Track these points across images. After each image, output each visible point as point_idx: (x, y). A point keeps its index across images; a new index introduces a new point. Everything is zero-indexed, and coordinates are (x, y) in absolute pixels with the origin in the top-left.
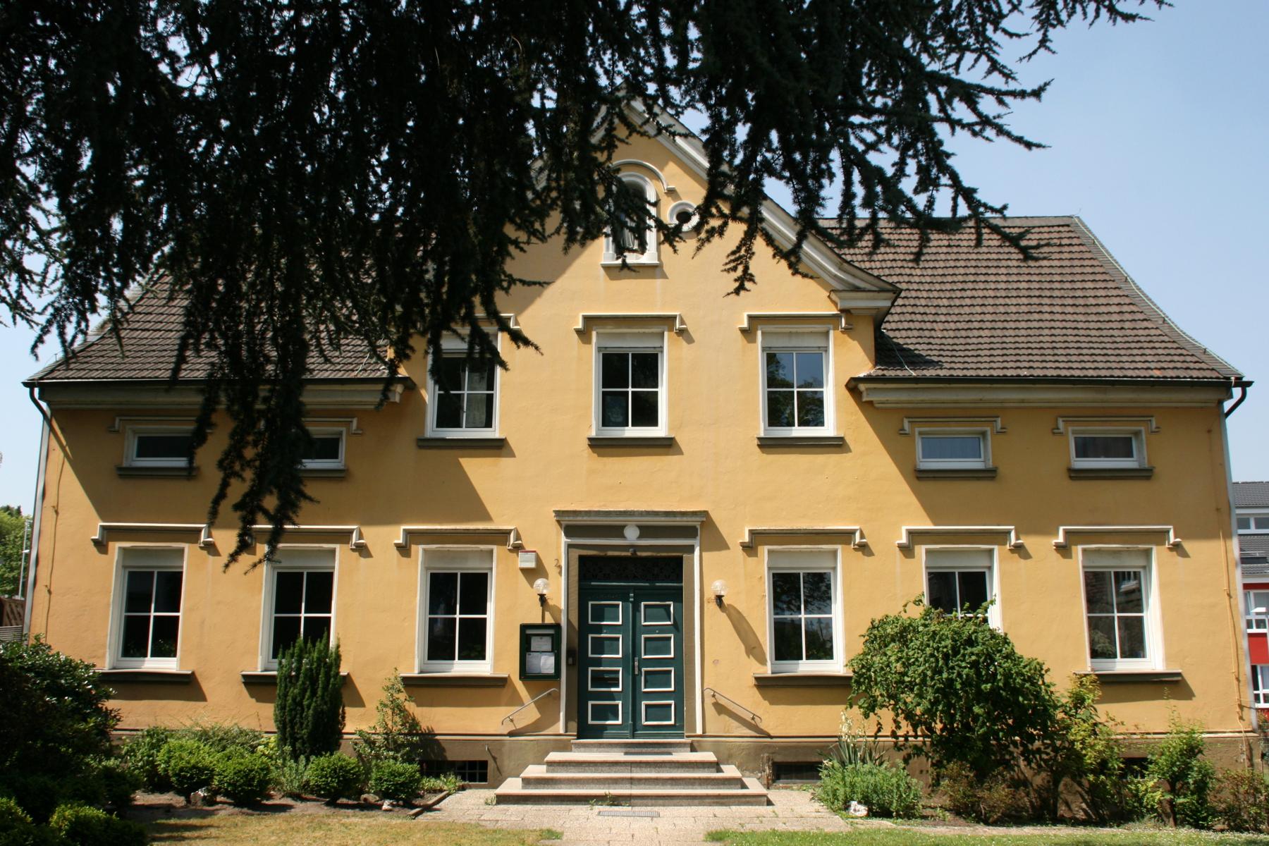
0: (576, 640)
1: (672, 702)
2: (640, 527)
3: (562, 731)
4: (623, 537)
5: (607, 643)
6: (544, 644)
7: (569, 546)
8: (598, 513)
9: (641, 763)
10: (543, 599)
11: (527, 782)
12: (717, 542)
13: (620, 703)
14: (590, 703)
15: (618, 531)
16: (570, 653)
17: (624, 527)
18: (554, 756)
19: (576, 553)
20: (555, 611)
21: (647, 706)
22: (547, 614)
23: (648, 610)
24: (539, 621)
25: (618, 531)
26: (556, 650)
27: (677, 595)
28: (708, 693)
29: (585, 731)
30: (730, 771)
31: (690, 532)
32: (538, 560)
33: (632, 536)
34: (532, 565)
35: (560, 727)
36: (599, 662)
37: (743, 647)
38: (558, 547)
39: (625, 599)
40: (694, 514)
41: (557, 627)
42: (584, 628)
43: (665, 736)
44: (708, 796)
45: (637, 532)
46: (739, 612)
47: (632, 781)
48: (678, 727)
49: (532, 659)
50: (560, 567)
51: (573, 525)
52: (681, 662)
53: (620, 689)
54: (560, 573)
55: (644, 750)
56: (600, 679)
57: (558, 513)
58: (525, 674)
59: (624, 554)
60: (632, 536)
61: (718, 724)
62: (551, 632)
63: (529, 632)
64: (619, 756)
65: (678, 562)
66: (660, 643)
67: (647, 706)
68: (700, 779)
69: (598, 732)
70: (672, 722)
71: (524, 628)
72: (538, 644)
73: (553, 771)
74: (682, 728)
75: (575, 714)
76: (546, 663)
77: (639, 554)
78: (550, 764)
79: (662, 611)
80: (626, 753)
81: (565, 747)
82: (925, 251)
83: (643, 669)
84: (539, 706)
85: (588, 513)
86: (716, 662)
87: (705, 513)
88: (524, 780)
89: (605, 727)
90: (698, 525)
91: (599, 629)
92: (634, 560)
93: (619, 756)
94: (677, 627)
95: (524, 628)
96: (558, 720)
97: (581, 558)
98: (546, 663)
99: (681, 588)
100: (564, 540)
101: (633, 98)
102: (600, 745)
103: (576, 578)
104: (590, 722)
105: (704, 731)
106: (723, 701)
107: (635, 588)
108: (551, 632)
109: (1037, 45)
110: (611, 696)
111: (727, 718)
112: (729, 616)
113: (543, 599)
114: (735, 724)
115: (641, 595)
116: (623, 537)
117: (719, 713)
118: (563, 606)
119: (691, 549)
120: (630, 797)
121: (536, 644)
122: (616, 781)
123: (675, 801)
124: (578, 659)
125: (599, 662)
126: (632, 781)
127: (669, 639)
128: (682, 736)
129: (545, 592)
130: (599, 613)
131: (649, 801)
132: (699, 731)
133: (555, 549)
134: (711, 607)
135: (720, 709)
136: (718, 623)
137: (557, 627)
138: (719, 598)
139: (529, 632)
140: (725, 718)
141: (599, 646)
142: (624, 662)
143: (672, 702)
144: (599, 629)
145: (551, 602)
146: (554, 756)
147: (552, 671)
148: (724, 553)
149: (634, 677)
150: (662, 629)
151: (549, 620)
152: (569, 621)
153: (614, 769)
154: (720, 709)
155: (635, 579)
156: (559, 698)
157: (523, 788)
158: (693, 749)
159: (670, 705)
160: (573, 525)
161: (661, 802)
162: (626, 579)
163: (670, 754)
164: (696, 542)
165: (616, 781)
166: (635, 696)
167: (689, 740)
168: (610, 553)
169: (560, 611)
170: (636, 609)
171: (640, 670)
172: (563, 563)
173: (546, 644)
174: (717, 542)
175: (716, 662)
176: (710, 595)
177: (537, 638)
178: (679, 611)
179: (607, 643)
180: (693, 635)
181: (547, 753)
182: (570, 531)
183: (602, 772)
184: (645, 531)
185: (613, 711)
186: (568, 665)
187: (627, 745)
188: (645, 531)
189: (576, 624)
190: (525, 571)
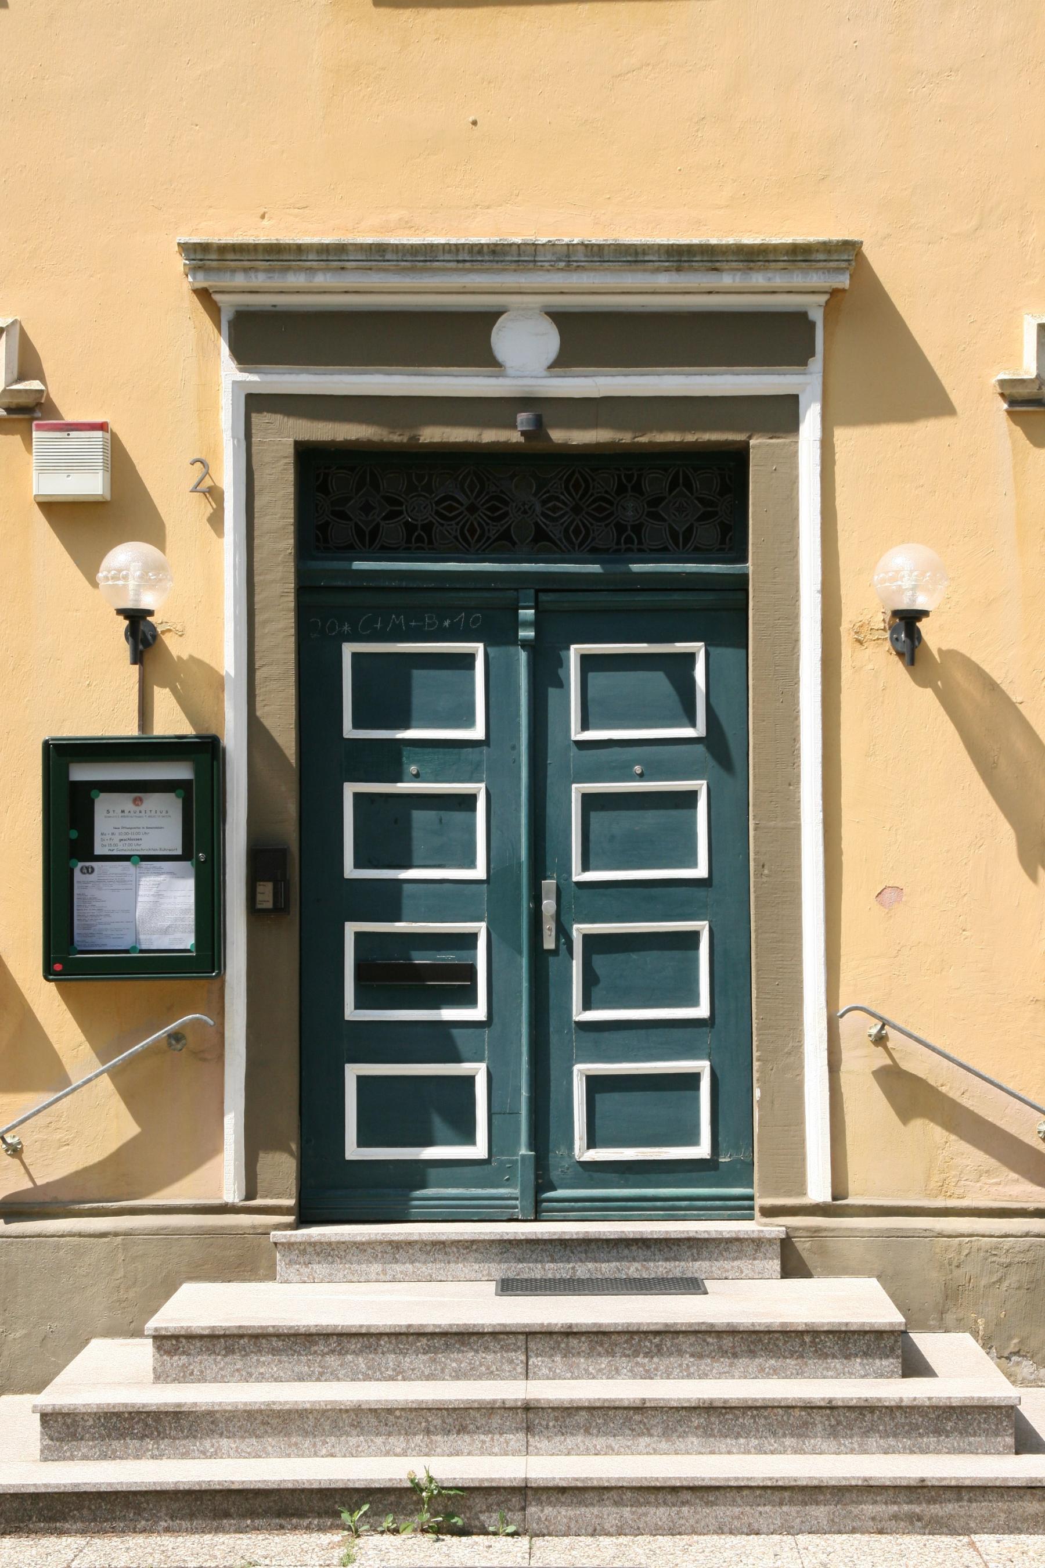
0: (292, 808)
1: (702, 1066)
2: (561, 318)
3: (231, 1192)
4: (485, 358)
5: (420, 818)
6: (137, 822)
7: (256, 403)
8: (379, 255)
9: (569, 1333)
10: (141, 631)
11: (64, 1429)
12: (908, 389)
13: (479, 1071)
14: (353, 1072)
15: (464, 335)
16: (262, 860)
17: (490, 317)
18: (200, 1305)
19: (283, 434)
20: (196, 684)
21: (594, 1083)
22: (163, 699)
23: (597, 679)
24: (128, 728)
25: (464, 335)
26: (201, 848)
27: (723, 614)
28: (856, 1029)
29: (329, 1193)
30: (960, 1367)
31: (780, 337)
32: (119, 463)
33: (525, 357)
34: (91, 484)
35: (224, 1176)
36: (387, 900)
37: (1006, 834)
38: (206, 409)
39: (497, 632)
40: (800, 255)
41: (205, 750)
42: (322, 755)
43: (671, 1209)
44: (869, 1490)
45: (548, 341)
46: (991, 686)
47: (531, 1419)
48: (726, 1172)
49: (96, 889)
50: (214, 494)
51: (272, 314)
52: (736, 897)
53: (478, 1013)
54: (216, 520)
55: (584, 1270)
56: (393, 973)
57: (202, 256)
58: (67, 954)
59: (490, 436)
60: (525, 357)
61: (897, 1159)
62: (180, 772)
63: (82, 773)
64: (470, 1300)
65: (733, 464)
66: (650, 819)
67: (594, 1083)
68: (830, 1408)
69: (384, 1195)
70: (702, 1150)
71: (59, 755)
72: (137, 822)
73: (185, 1376)
74: (743, 1173)
75: (288, 1120)
76: (159, 908)
77: (558, 436)
78: (170, 1343)
79: (658, 681)
80: (508, 1287)
81: (244, 1261)
82: (152, 899)
83: (579, 930)
84: (135, 1088)
85: (333, 255)
86: (887, 896)
87: (848, 254)
88: (48, 1418)
89: (417, 1174)
90: (815, 308)
91: (388, 760)
92: (537, 461)
93: (470, 1300)
94: (722, 750)
95: (59, 755)
96: (215, 1148)
97: (308, 456)
98: (159, 908)
99: (741, 584)
100: (229, 376)
101: (549, 951)
102: (397, 1248)
103: (288, 543)
104: (353, 1151)
105: (839, 1191)
106: (918, 1063)
107: (543, 585)
108: (180, 772)
109: (17, 1161)
110: (441, 1042)
111: (937, 1133)
112: (948, 701)
113: (141, 631)
114: (971, 1157)
115: (569, 613)
116: (485, 358)
117: (906, 1112)
118: (228, 660)
119: (783, 414)
120: (524, 1493)
121: (114, 823)
122: (459, 1421)
123: (723, 1512)
124: (299, 886)
125: (387, 900)
126: (531, 1419)
127: (689, 799)
128: (743, 1208)
129: (147, 601)
130: (388, 694)
131: (610, 1514)
132: (818, 1189)
133: (192, 415)
134: (872, 664)
135: (910, 1095)
136: (895, 724)
137: (205, 750)
138: (907, 623)
139: (82, 773)
140: (929, 1133)
141: (390, 832)
142: (496, 895)
143: (702, 1066)
144: (388, 760)
145: (175, 646)
146: (200, 1305)
147: (185, 940)
148: (928, 428)
149: (539, 957)
150: (658, 757)
151: (170, 721)
152: (256, 729)
153: (454, 1360)
154: (910, 1095)
155: (542, 544)
156: (213, 1052)
157: (48, 1455)
158: (793, 1264)
159: (692, 1080)
160: (272, 314)
161: (660, 1514)
162: (502, 546)
163: (693, 1286)
164: (805, 383)
165: (459, 1421)
166: (545, 1043)
167: (775, 1228)
168: (432, 434)
169: (218, 683)
170: (546, 674)
171: (563, 932)
172: (228, 477)
173: (160, 824)
174: (908, 389)
175: (887, 896)
176: (866, 608)
177: (124, 801)
178: (731, 686)
179: (420, 818)
180: (794, 781)
181: (168, 1288)
182: (255, 335)
183: (399, 1374)
184: (587, 336)
185: (452, 1107)
186: (253, 910)
187: (507, 1247)
188: (587, 336)
189: (287, 739)
190: (61, 512)
